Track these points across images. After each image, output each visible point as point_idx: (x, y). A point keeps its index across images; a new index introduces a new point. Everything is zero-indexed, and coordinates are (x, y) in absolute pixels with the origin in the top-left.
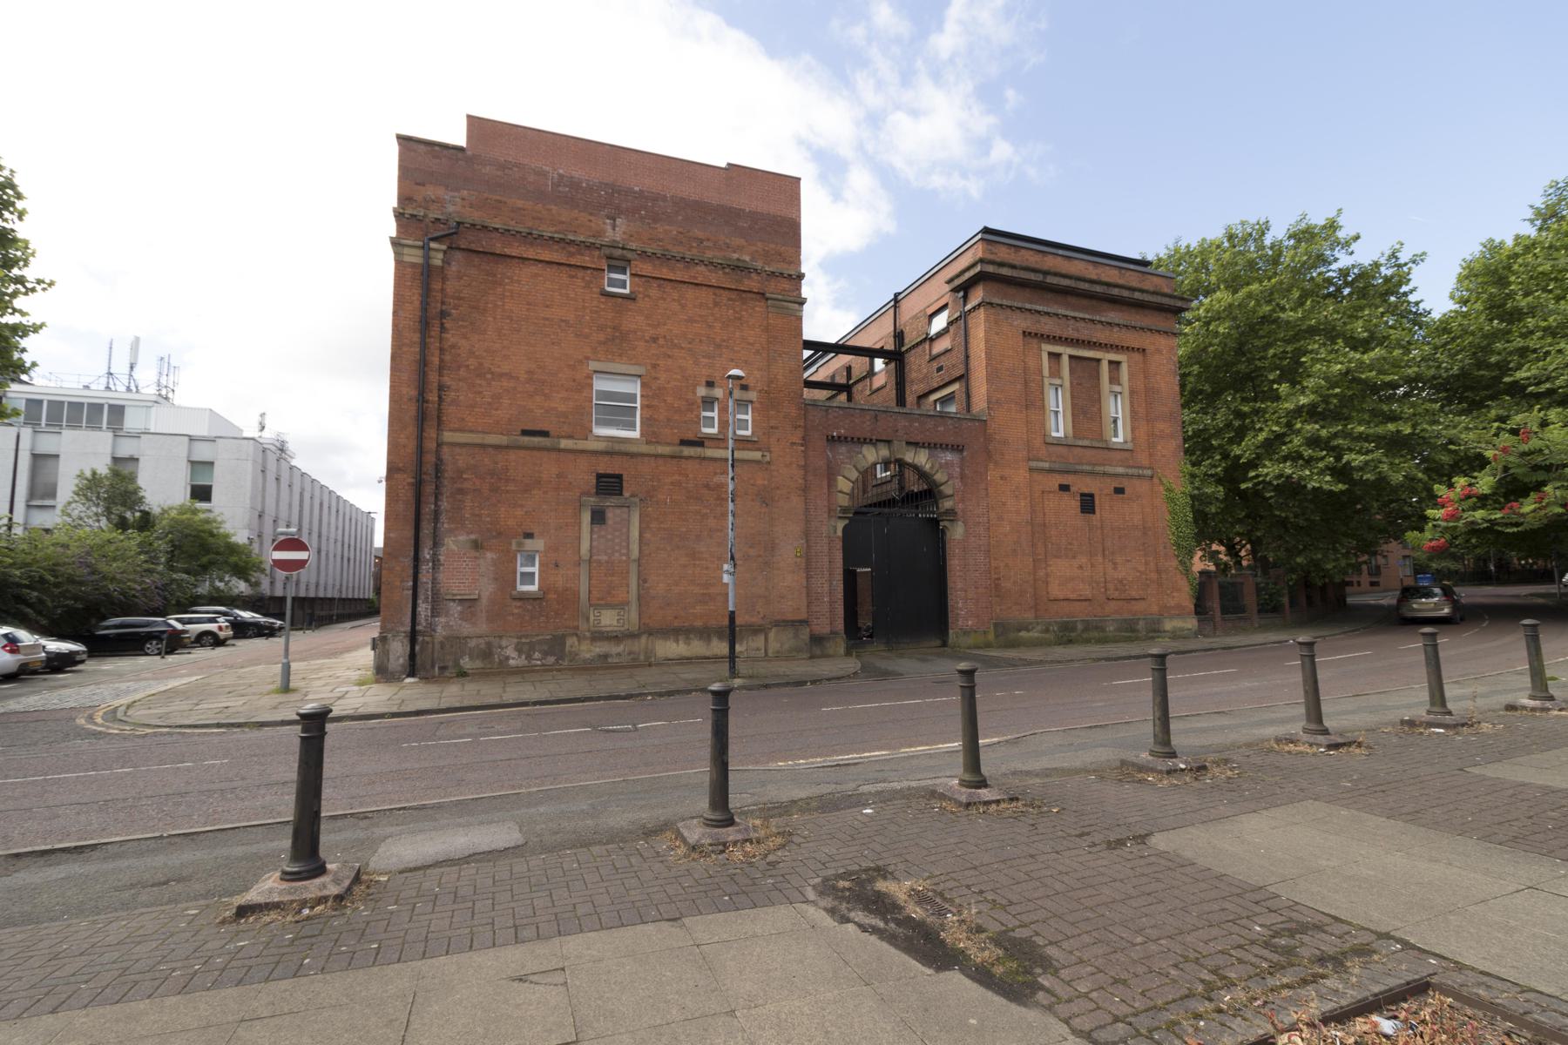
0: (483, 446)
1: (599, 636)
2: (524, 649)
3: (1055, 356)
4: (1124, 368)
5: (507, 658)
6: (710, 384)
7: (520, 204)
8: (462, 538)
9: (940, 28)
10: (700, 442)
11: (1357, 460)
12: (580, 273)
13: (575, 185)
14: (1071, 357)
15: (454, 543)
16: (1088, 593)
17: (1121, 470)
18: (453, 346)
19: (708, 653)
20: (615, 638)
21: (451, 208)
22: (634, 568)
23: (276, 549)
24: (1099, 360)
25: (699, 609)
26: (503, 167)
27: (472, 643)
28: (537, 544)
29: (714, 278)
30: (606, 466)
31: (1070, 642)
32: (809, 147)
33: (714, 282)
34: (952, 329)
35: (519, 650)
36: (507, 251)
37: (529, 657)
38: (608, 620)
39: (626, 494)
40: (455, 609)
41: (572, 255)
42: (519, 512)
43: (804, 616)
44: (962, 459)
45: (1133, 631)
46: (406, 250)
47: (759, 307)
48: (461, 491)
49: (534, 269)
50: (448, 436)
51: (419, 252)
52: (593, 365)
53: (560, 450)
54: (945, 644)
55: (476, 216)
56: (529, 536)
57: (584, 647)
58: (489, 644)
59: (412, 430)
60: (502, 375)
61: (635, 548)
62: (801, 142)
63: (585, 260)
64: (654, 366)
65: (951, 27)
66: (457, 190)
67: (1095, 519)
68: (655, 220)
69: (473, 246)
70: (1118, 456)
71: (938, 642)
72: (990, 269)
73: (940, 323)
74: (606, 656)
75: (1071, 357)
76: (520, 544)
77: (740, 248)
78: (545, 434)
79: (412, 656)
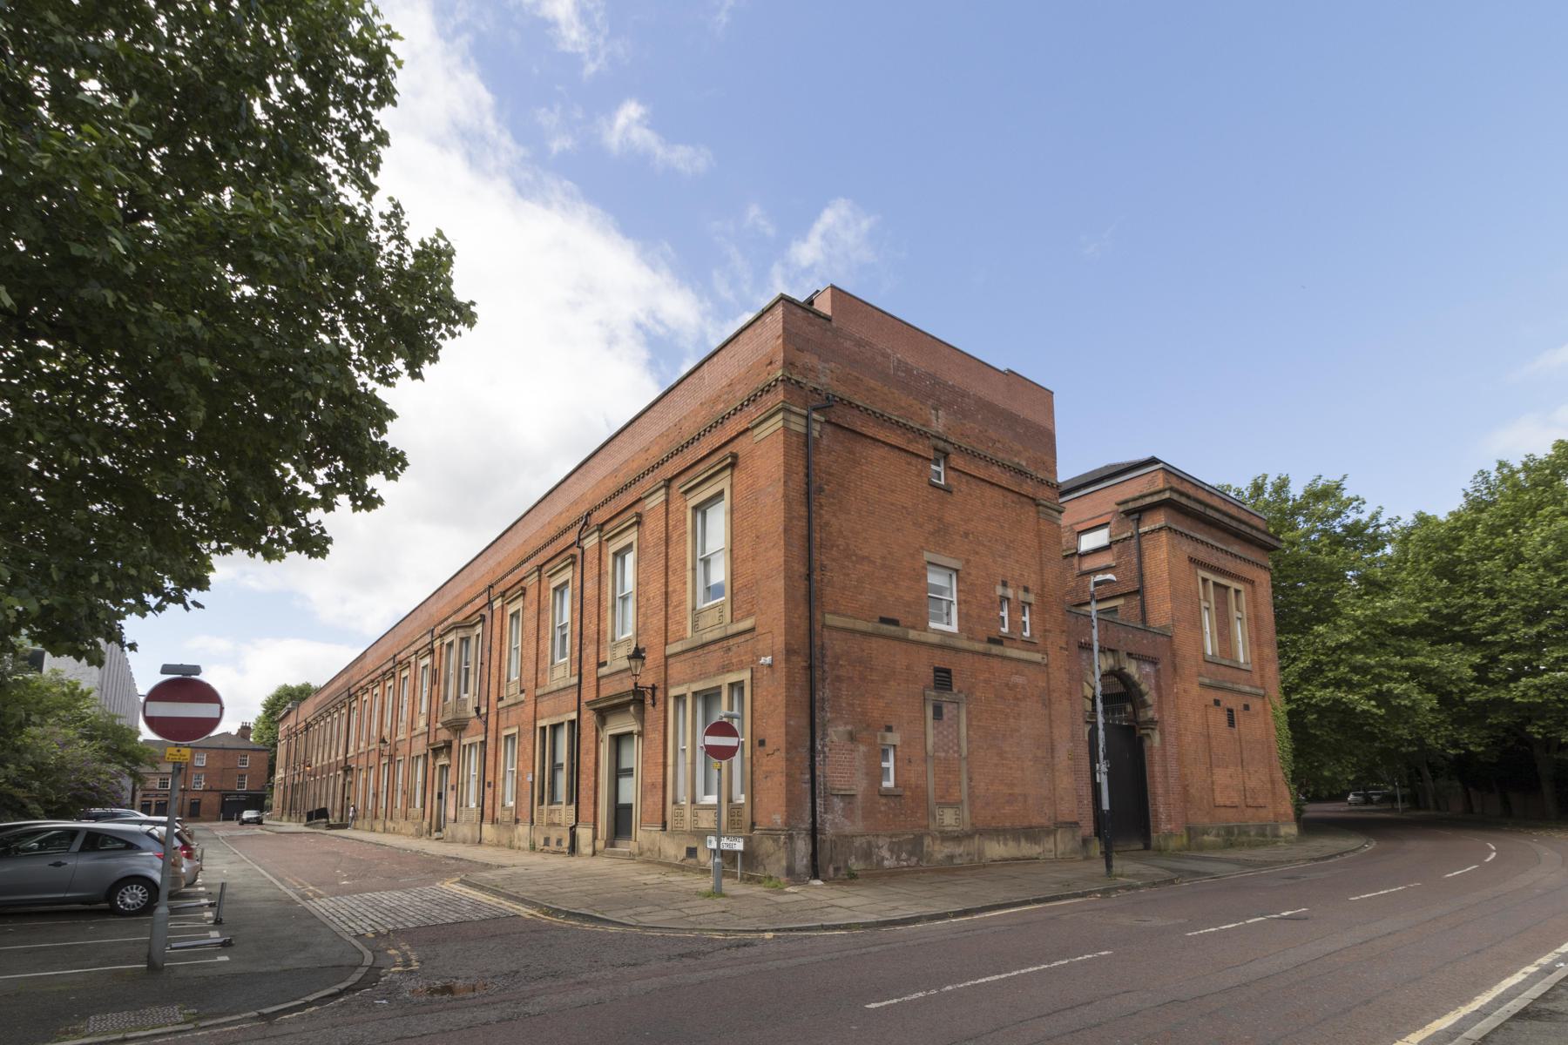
0: (853, 631)
1: (947, 837)
2: (895, 849)
3: (1205, 580)
4: (1243, 595)
5: (883, 859)
6: (1004, 584)
7: (872, 383)
8: (841, 729)
9: (804, 237)
10: (998, 641)
11: (1399, 689)
12: (914, 460)
13: (909, 371)
14: (1215, 584)
15: (836, 733)
16: (1236, 800)
17: (1247, 689)
18: (827, 524)
19: (1019, 855)
20: (957, 838)
21: (823, 380)
22: (964, 765)
23: (707, 734)
24: (1227, 588)
25: (1007, 810)
26: (859, 343)
27: (858, 842)
28: (894, 738)
29: (1005, 479)
30: (942, 660)
31: (1232, 845)
32: (647, 333)
33: (1004, 484)
34: (1115, 548)
35: (891, 851)
36: (865, 430)
37: (898, 859)
38: (949, 818)
39: (955, 690)
40: (838, 804)
41: (910, 441)
42: (881, 704)
43: (1076, 819)
44: (1158, 671)
45: (1264, 835)
46: (793, 418)
47: (1031, 511)
48: (838, 679)
49: (883, 451)
50: (831, 619)
51: (803, 422)
52: (927, 556)
53: (908, 641)
54: (1147, 847)
55: (842, 391)
56: (889, 729)
57: (936, 848)
58: (869, 843)
59: (802, 609)
60: (864, 558)
61: (964, 744)
62: (639, 326)
63: (919, 447)
64: (968, 561)
65: (815, 240)
66: (826, 361)
67: (1235, 730)
68: (965, 417)
69: (840, 422)
70: (1244, 675)
71: (1141, 846)
72: (1175, 497)
73: (1099, 538)
74: (951, 857)
75: (1215, 584)
76: (883, 738)
77: (1018, 454)
78: (895, 622)
79: (814, 855)
